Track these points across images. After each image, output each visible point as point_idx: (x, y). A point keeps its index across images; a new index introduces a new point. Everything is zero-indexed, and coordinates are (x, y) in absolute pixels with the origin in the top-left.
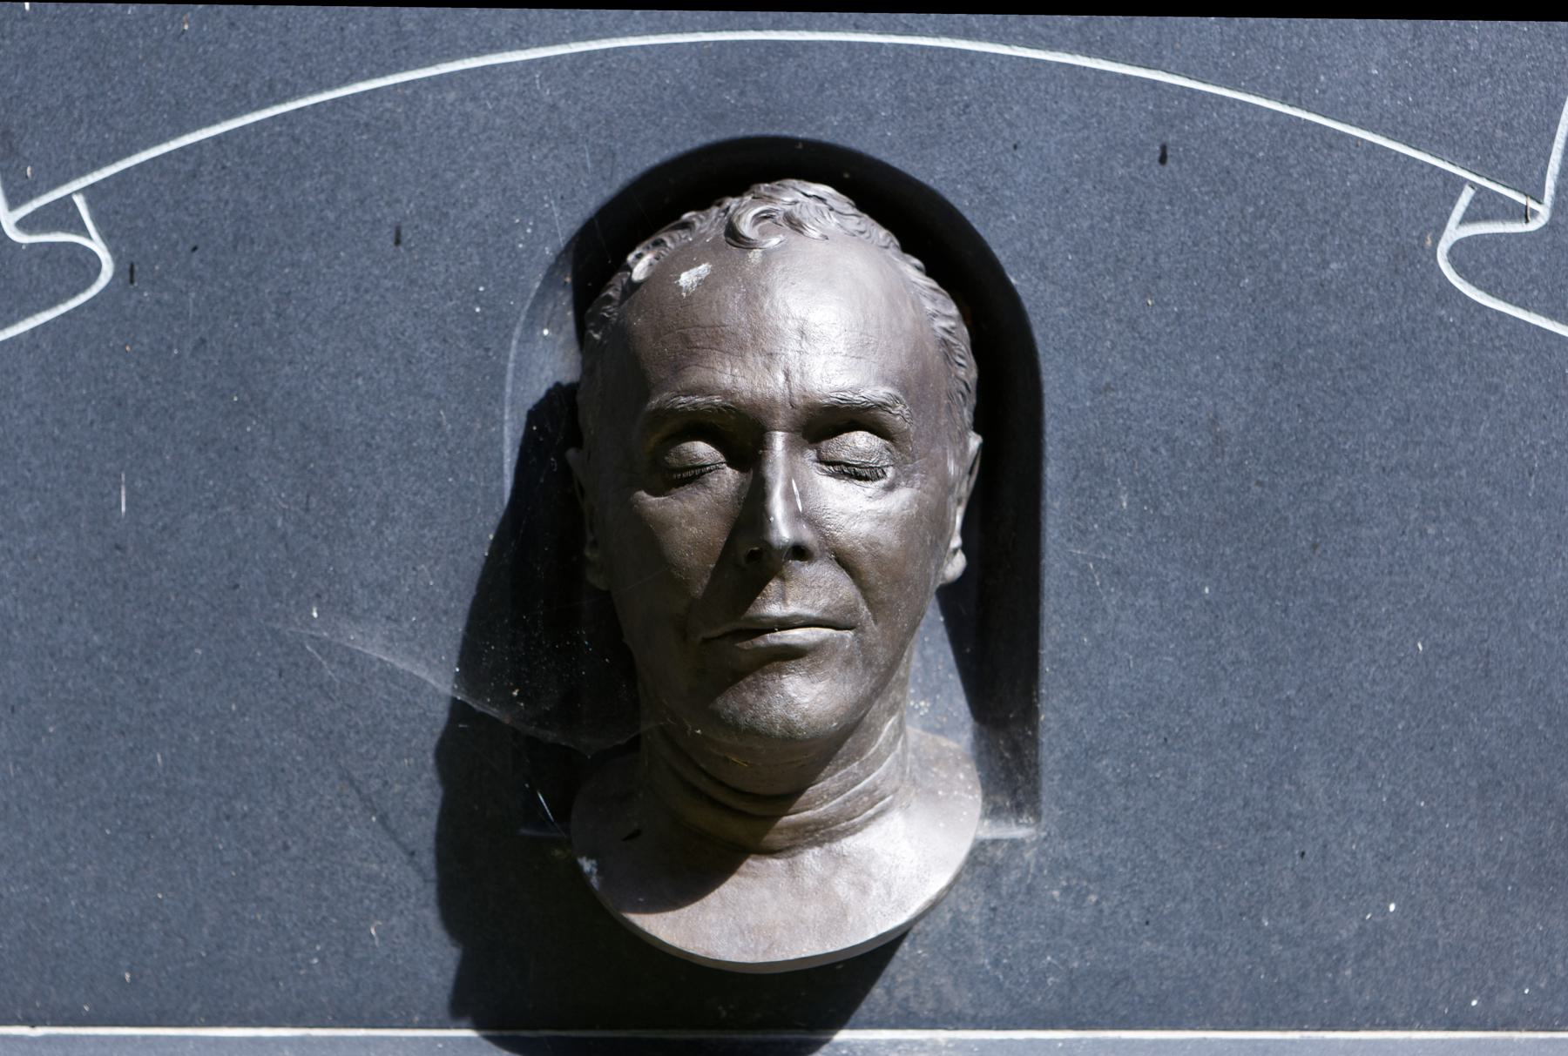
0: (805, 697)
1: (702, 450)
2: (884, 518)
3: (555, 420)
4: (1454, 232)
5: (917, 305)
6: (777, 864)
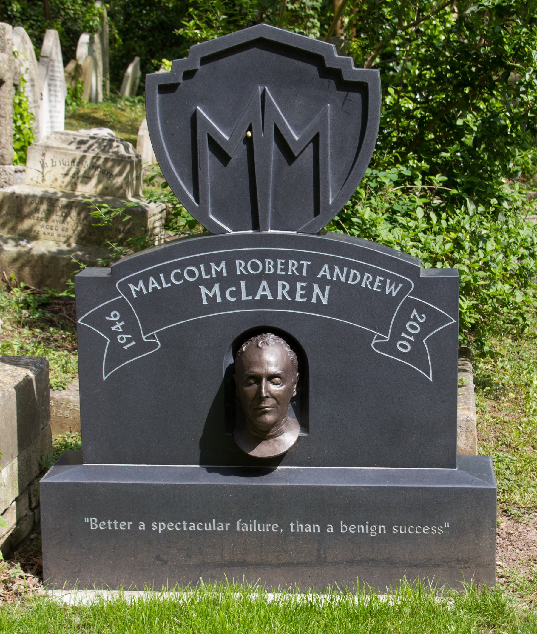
0: (269, 418)
1: (252, 381)
2: (281, 391)
3: (231, 369)
4: (374, 341)
5: (287, 355)
6: (266, 441)
